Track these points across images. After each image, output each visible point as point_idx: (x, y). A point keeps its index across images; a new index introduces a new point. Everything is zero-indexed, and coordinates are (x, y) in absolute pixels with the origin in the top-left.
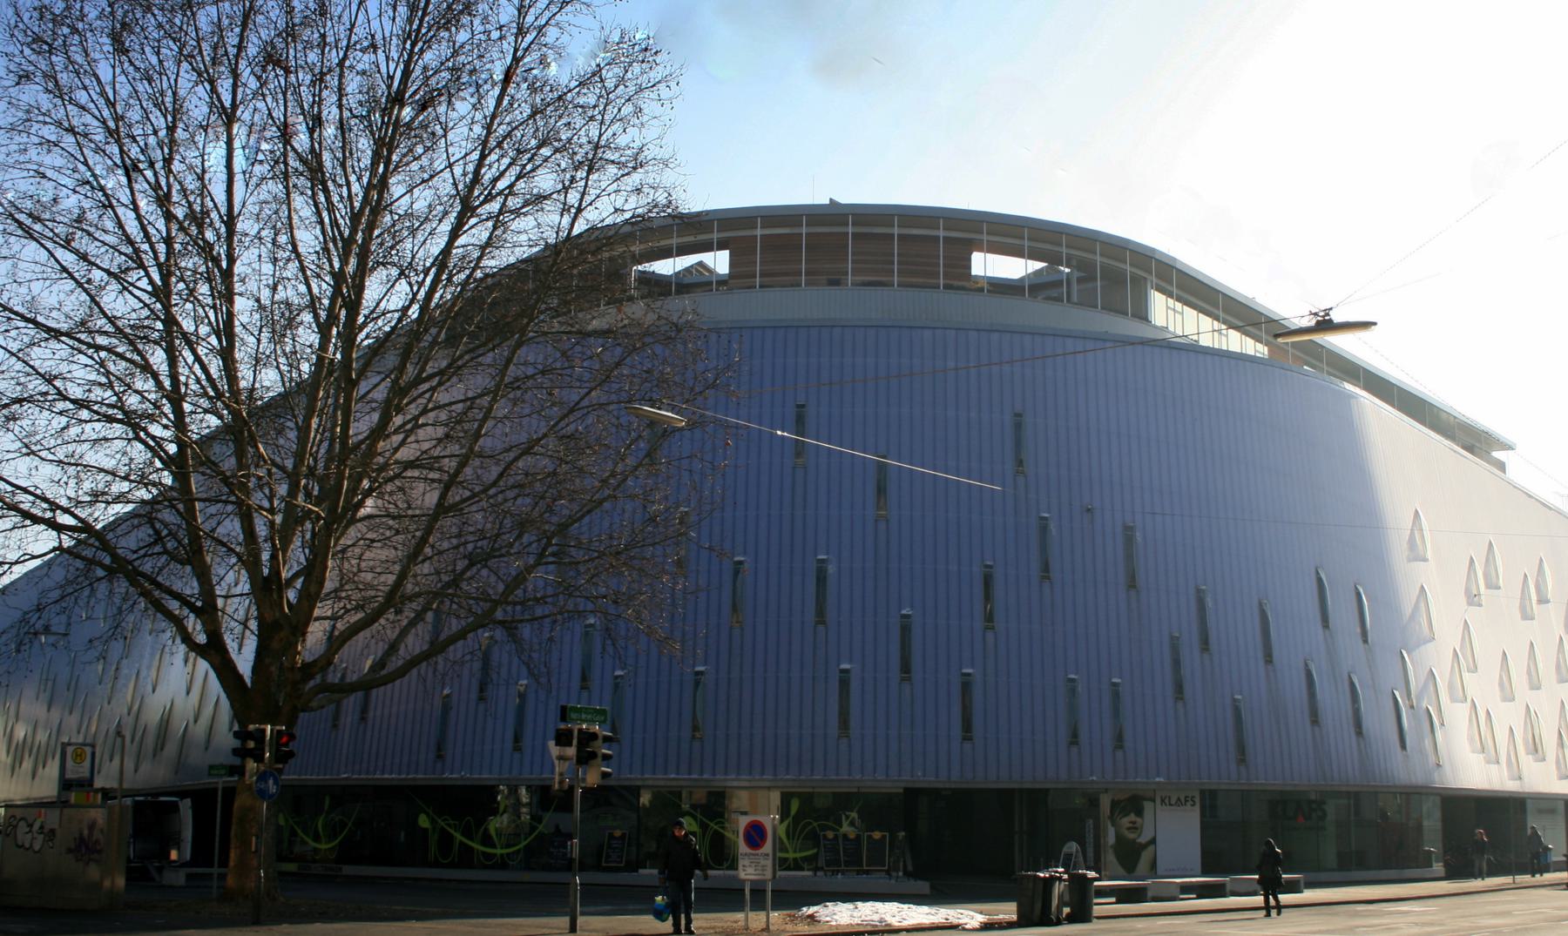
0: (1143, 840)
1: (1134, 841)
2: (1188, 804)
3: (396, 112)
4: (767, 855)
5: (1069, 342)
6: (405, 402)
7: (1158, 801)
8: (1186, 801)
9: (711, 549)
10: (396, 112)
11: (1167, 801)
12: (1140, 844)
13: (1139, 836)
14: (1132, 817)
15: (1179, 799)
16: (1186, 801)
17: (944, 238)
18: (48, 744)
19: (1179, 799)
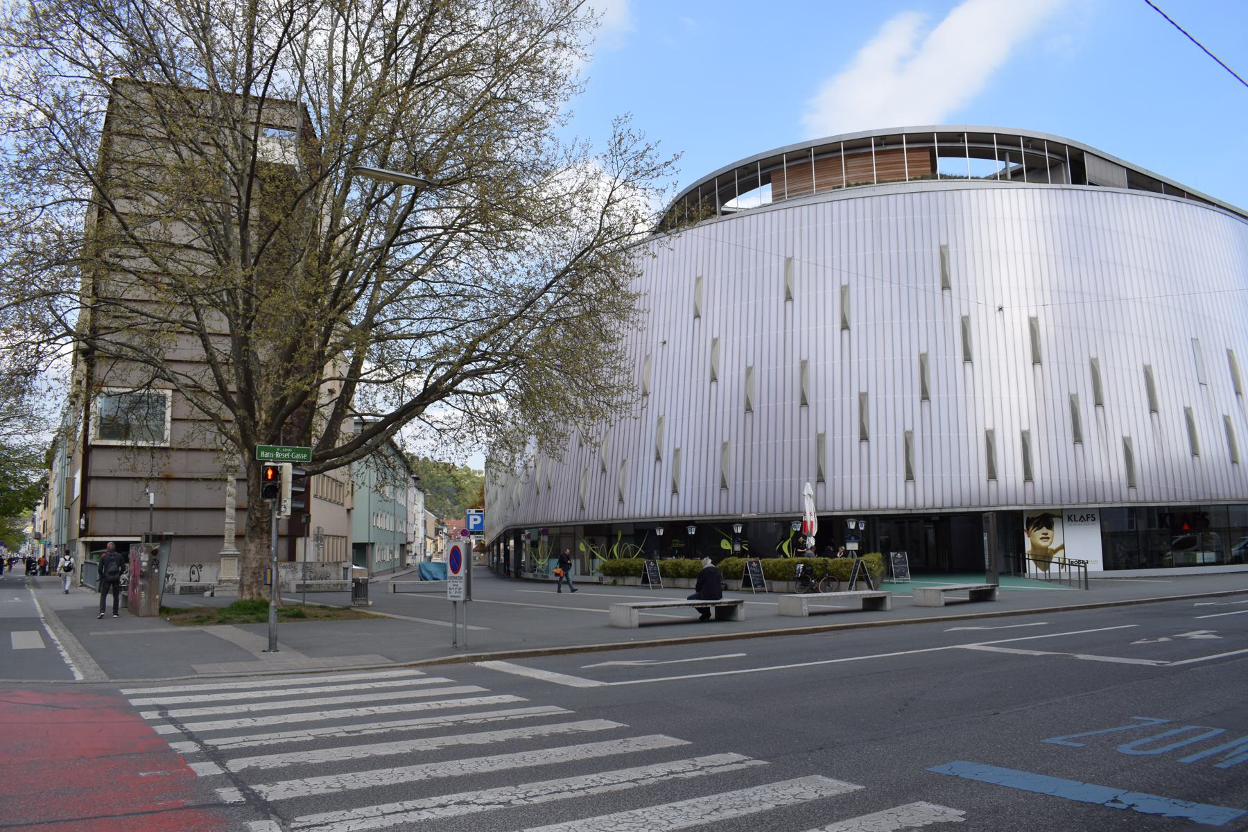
0: (1054, 546)
1: (1047, 548)
2: (1090, 519)
3: (502, 557)
4: (461, 578)
5: (144, 317)
6: (474, 226)
7: (1065, 518)
8: (1088, 518)
9: (636, 419)
10: (502, 557)
11: (1072, 518)
12: (1052, 550)
13: (1051, 543)
14: (1044, 530)
15: (1082, 516)
16: (1088, 518)
17: (309, 450)
18: (1218, 457)
19: (1082, 516)
